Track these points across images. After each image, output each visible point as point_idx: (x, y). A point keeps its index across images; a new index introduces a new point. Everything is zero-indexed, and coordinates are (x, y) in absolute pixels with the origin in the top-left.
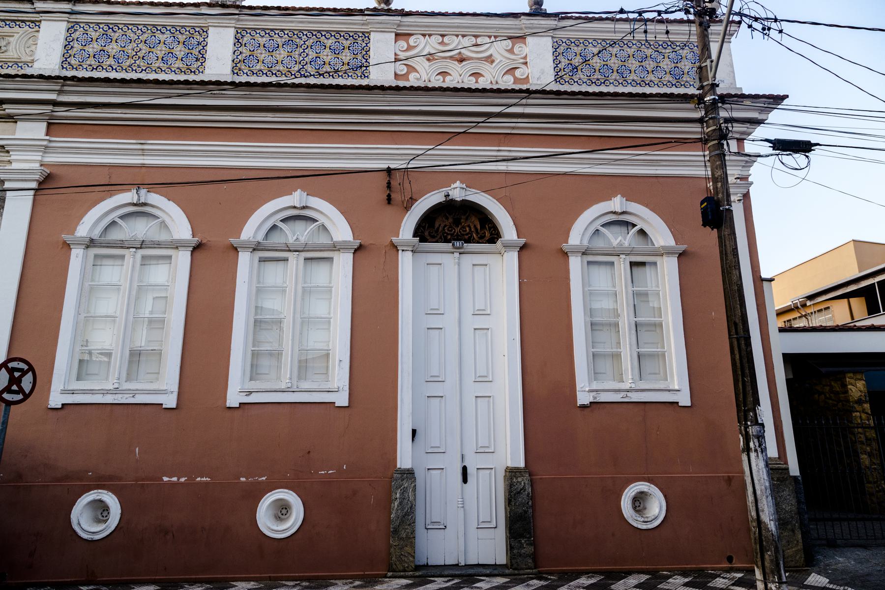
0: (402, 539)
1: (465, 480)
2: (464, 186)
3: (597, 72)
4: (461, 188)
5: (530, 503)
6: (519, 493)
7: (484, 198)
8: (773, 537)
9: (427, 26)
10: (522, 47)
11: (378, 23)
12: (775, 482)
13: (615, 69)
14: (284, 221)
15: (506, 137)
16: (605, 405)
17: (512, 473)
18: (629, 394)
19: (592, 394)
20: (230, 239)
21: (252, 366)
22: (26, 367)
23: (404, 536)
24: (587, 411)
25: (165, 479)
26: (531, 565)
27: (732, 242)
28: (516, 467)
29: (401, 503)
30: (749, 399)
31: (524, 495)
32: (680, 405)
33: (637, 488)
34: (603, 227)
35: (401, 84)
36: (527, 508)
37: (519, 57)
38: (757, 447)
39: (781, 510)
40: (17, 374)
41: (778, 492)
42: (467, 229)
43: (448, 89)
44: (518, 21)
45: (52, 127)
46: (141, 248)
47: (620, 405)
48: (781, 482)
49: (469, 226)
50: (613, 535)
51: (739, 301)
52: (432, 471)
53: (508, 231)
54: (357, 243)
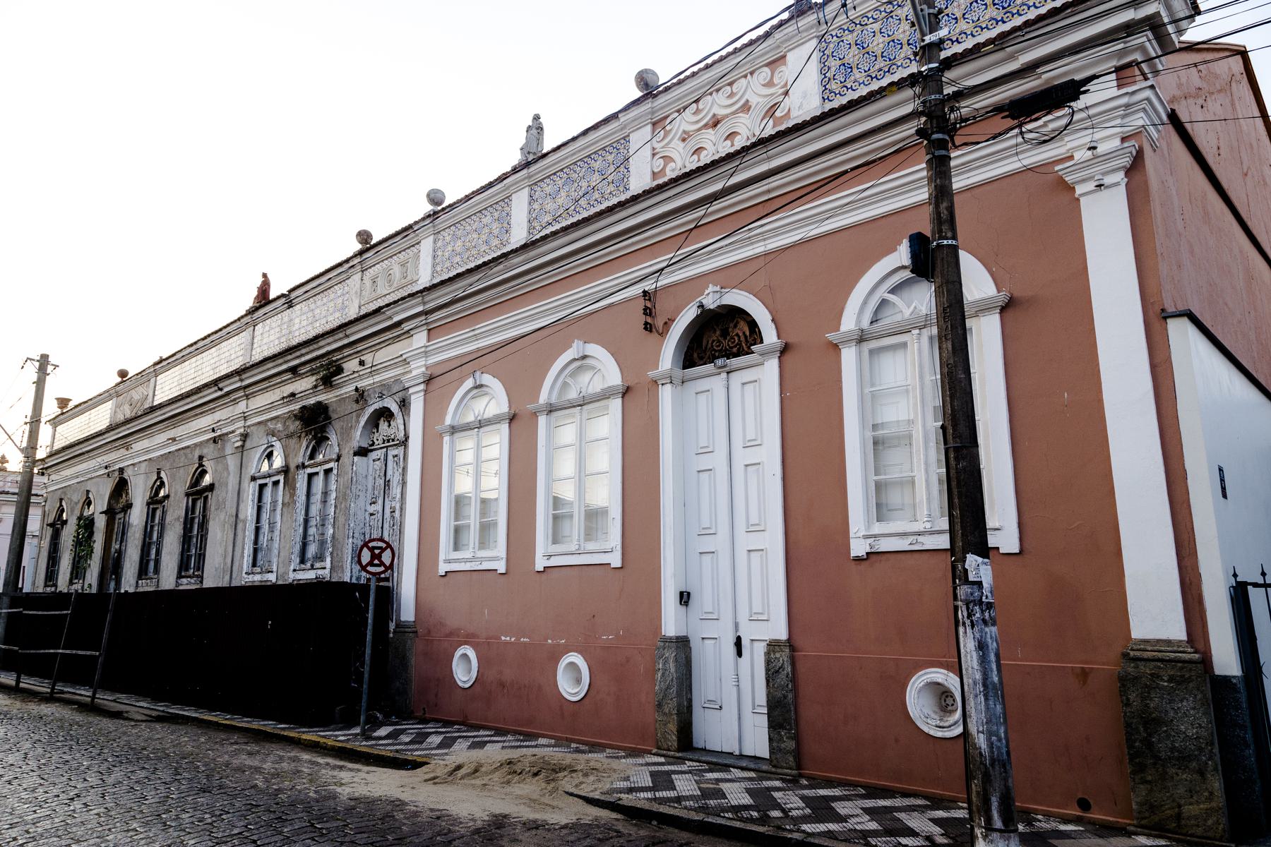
0: (665, 714)
1: (739, 654)
2: (718, 288)
3: (879, 58)
4: (714, 292)
5: (790, 686)
6: (777, 672)
7: (739, 296)
8: (981, 758)
9: (679, 99)
10: (782, 71)
11: (633, 121)
12: (1166, 684)
13: (905, 42)
14: (893, 291)
15: (764, 206)
16: (888, 555)
17: (773, 646)
18: (920, 539)
19: (869, 541)
20: (827, 335)
21: (878, 505)
22: (384, 545)
23: (667, 711)
24: (864, 565)
25: (503, 638)
26: (792, 764)
27: (944, 297)
28: (776, 640)
29: (663, 675)
30: (958, 545)
31: (783, 675)
32: (1002, 551)
33: (923, 679)
34: (893, 294)
35: (660, 181)
36: (787, 692)
37: (779, 86)
38: (965, 619)
39: (1177, 733)
40: (377, 552)
41: (1171, 701)
42: (736, 338)
43: (745, 150)
44: (771, 40)
45: (431, 332)
46: (481, 427)
47: (908, 555)
48: (1179, 683)
49: (737, 335)
50: (897, 741)
51: (949, 391)
52: (707, 642)
53: (770, 335)
54: (1003, 297)
